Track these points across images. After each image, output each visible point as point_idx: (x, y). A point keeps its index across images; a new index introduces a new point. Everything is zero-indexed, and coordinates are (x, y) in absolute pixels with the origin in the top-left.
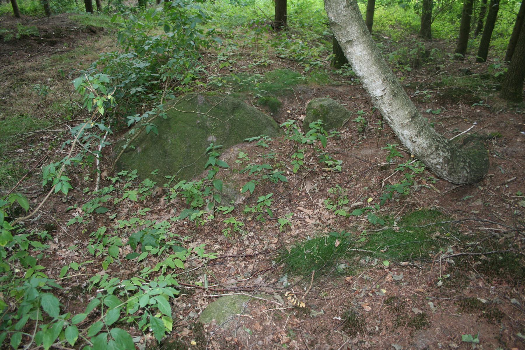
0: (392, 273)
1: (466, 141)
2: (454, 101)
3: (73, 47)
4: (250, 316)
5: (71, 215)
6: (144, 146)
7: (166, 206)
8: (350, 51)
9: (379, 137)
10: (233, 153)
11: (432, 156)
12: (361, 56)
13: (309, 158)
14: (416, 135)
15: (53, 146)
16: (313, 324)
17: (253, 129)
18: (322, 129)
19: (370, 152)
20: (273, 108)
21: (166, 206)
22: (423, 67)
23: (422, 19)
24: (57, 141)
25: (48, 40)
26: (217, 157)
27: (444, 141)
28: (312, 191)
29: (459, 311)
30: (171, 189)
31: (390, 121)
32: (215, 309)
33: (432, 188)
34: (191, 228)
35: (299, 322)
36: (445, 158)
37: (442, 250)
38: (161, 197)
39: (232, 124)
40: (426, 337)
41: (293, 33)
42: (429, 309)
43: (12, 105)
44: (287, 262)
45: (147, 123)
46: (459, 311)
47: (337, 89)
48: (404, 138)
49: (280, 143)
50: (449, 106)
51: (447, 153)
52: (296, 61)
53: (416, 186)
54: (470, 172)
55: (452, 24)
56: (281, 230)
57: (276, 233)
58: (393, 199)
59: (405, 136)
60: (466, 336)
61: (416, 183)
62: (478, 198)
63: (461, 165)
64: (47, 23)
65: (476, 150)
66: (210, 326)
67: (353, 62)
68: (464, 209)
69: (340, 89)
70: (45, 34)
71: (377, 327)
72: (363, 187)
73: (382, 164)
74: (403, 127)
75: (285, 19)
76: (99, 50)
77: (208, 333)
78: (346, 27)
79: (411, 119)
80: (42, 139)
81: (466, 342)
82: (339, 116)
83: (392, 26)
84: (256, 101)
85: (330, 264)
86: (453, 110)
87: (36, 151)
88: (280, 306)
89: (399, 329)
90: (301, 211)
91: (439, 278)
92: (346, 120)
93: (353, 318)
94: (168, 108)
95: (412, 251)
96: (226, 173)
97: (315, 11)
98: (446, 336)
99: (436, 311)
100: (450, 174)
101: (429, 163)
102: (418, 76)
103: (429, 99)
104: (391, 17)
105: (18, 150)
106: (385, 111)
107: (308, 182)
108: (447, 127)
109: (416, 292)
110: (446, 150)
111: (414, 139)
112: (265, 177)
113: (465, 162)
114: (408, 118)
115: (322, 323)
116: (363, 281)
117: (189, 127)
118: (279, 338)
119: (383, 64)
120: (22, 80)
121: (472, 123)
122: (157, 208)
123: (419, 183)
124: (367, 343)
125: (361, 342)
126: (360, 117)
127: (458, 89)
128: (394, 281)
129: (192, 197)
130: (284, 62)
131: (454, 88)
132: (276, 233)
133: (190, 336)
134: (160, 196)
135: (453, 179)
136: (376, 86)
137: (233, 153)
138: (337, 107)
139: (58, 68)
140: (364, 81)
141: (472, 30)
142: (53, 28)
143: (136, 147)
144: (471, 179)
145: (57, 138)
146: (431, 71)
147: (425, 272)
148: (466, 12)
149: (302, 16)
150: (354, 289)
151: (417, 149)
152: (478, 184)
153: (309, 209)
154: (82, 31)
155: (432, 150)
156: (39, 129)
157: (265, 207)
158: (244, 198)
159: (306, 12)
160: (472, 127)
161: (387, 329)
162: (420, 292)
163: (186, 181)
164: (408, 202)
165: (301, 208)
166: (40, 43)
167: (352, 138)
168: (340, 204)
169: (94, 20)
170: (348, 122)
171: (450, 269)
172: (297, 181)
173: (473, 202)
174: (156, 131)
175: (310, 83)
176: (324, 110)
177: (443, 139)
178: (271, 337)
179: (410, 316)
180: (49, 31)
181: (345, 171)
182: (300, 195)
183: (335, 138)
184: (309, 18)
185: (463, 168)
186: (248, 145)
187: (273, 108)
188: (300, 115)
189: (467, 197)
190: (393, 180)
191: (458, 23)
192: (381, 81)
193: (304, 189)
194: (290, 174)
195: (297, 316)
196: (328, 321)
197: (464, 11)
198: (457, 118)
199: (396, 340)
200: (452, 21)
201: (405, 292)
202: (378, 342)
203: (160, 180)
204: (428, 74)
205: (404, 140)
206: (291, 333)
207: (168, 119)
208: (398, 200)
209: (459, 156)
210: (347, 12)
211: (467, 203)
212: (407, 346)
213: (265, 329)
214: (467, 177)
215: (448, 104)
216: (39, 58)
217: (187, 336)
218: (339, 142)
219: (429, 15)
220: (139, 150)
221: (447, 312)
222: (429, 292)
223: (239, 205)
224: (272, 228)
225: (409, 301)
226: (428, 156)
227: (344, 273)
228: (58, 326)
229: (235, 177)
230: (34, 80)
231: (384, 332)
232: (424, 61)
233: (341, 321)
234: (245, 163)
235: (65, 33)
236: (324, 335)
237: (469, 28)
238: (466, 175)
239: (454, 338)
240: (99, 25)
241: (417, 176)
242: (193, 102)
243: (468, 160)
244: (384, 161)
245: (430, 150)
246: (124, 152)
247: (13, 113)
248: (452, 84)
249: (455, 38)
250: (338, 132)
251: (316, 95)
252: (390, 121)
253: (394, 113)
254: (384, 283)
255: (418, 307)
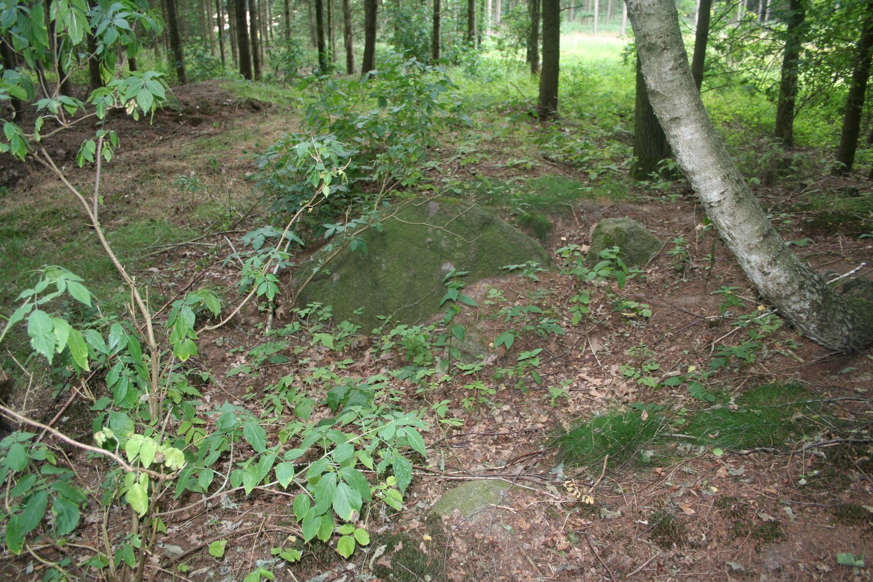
0: (728, 466)
1: (847, 287)
2: (829, 231)
3: (226, 129)
4: (511, 509)
5: (229, 365)
6: (343, 271)
7: (373, 363)
8: (675, 133)
9: (708, 280)
10: (479, 291)
11: (793, 299)
12: (691, 140)
13: (597, 306)
14: (770, 264)
15: (202, 266)
16: (606, 528)
17: (511, 258)
18: (620, 261)
19: (693, 300)
20: (541, 231)
21: (373, 363)
22: (779, 184)
23: (779, 109)
24: (208, 260)
25: (189, 116)
26: (459, 289)
27: (812, 277)
28: (601, 353)
29: (832, 521)
30: (384, 338)
31: (730, 239)
32: (459, 495)
33: (791, 356)
34: (412, 397)
35: (584, 523)
36: (813, 303)
37: (805, 437)
38: (365, 350)
39: (480, 247)
40: (780, 554)
41: (566, 125)
42: (786, 517)
43: (138, 206)
44: (567, 448)
45: (353, 237)
46: (832, 521)
47: (641, 208)
48: (751, 267)
49: (552, 282)
50: (821, 238)
51: (817, 295)
52: (574, 166)
53: (765, 352)
54: (853, 329)
55: (829, 123)
56: (552, 404)
57: (544, 410)
58: (729, 368)
59: (753, 264)
60: (844, 555)
61: (765, 347)
62: (865, 371)
63: (839, 317)
64: (188, 92)
65: (864, 300)
66: (452, 519)
67: (680, 149)
68: (842, 386)
69: (646, 209)
70: (185, 107)
71: (703, 535)
72: (681, 350)
73: (712, 318)
74: (750, 249)
75: (555, 103)
76: (267, 134)
77: (448, 527)
78: (671, 98)
79: (762, 238)
80: (185, 256)
81: (843, 565)
82: (644, 248)
83: (728, 124)
84: (513, 219)
85: (630, 449)
86: (828, 244)
87: (176, 271)
88: (555, 498)
89: (738, 541)
90: (584, 380)
91: (801, 476)
92: (655, 254)
93: (666, 523)
94: (383, 217)
95: (759, 436)
96: (468, 319)
97: (601, 94)
98: (811, 554)
99: (795, 519)
100: (821, 329)
101: (788, 310)
102: (770, 196)
103: (790, 227)
104: (725, 108)
105: (151, 269)
106: (723, 225)
107: (595, 340)
108: (818, 268)
109: (765, 493)
110: (815, 291)
111: (766, 270)
112: (531, 328)
113: (845, 312)
114: (758, 237)
115: (619, 527)
116: (682, 475)
117: (415, 248)
118: (554, 542)
119: (724, 155)
120: (153, 171)
121: (857, 263)
122: (359, 365)
123: (770, 347)
124: (687, 557)
125: (678, 556)
126: (678, 248)
127: (837, 214)
128: (731, 476)
129: (415, 351)
130: (554, 166)
131: (830, 213)
132: (544, 410)
133: (421, 531)
134: (364, 348)
135: (824, 339)
136: (712, 186)
137: (479, 291)
138: (641, 233)
139: (205, 156)
140: (694, 179)
141: (863, 135)
142: (197, 99)
143: (332, 272)
144: (855, 343)
145: (208, 255)
146: (791, 189)
147: (778, 466)
148: (852, 104)
149: (581, 102)
150: (669, 483)
151: (770, 286)
152: (866, 352)
153: (596, 378)
154: (239, 106)
155: (793, 289)
156: (180, 241)
157: (530, 369)
158: (495, 358)
159: (588, 96)
160: (858, 268)
161: (719, 541)
162: (770, 494)
163: (406, 326)
164: (751, 374)
165: (584, 375)
166: (177, 120)
167: (663, 281)
168: (646, 370)
169: (257, 91)
170: (658, 257)
171: (818, 464)
172: (578, 337)
173: (856, 376)
174: (365, 250)
175: (598, 198)
176: (620, 237)
177: (810, 274)
178: (543, 539)
179: (755, 523)
180: (192, 104)
181: (653, 326)
182: (582, 357)
183: (636, 280)
184: (592, 105)
185: (842, 322)
186: (503, 281)
187: (541, 231)
188: (581, 244)
189: (847, 370)
190: (728, 342)
191: (839, 122)
192: (719, 179)
193: (589, 349)
194: (568, 327)
195: (581, 515)
196: (629, 526)
197: (849, 101)
198: (834, 255)
199: (733, 556)
200: (828, 118)
201: (748, 492)
202: (705, 558)
203: (368, 322)
204: (787, 194)
205: (751, 271)
206: (572, 536)
207: (383, 234)
208: (735, 371)
209: (836, 302)
210: (675, 77)
211: (848, 378)
212: (750, 566)
213: (534, 528)
214: (848, 337)
215: (819, 235)
216: (176, 143)
217: (417, 530)
218: (643, 286)
219: (791, 104)
220: (336, 277)
221: (813, 522)
222: (784, 494)
223: (488, 367)
224: (538, 402)
225: (753, 504)
226: (787, 297)
227: (652, 463)
228: (267, 461)
229: (482, 325)
230: (171, 172)
231: (715, 544)
232: (782, 174)
233: (648, 526)
234: (496, 307)
235: (215, 108)
236: (622, 543)
237: (858, 130)
238: (847, 333)
239: (825, 558)
240: (264, 100)
241: (767, 337)
242: (422, 211)
243: (850, 311)
244: (715, 314)
245: (790, 288)
246: (312, 280)
247: (139, 217)
248: (827, 207)
249: (834, 146)
250: (642, 271)
251: (606, 216)
252: (730, 239)
253: (738, 228)
254: (714, 479)
255: (769, 513)
